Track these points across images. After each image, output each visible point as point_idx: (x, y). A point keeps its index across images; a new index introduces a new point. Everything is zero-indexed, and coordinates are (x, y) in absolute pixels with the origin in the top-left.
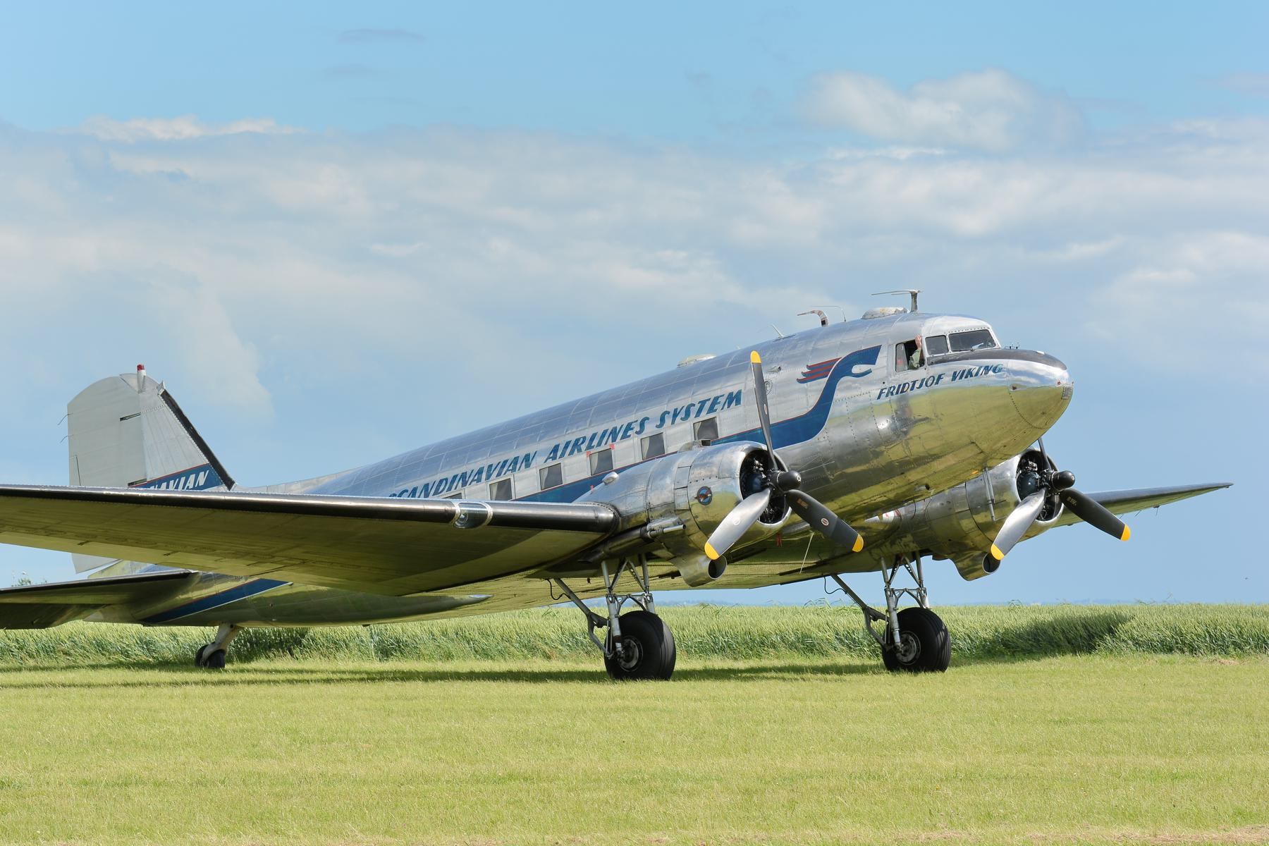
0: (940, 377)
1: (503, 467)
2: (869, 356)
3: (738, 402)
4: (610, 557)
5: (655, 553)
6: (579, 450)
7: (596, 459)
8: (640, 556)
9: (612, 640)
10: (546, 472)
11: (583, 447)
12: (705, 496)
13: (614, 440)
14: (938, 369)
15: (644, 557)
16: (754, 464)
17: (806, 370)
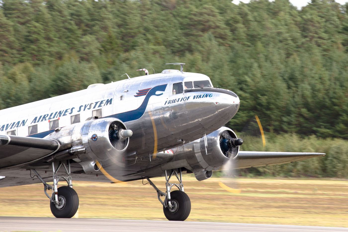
0: (189, 98)
1: (13, 125)
2: (163, 88)
3: (111, 103)
4: (55, 161)
5: (74, 159)
6: (45, 120)
7: (52, 124)
8: (67, 161)
9: (167, 200)
10: (31, 128)
11: (47, 118)
12: (95, 138)
13: (60, 116)
14: (188, 94)
15: (69, 161)
16: (114, 126)
17: (138, 92)
